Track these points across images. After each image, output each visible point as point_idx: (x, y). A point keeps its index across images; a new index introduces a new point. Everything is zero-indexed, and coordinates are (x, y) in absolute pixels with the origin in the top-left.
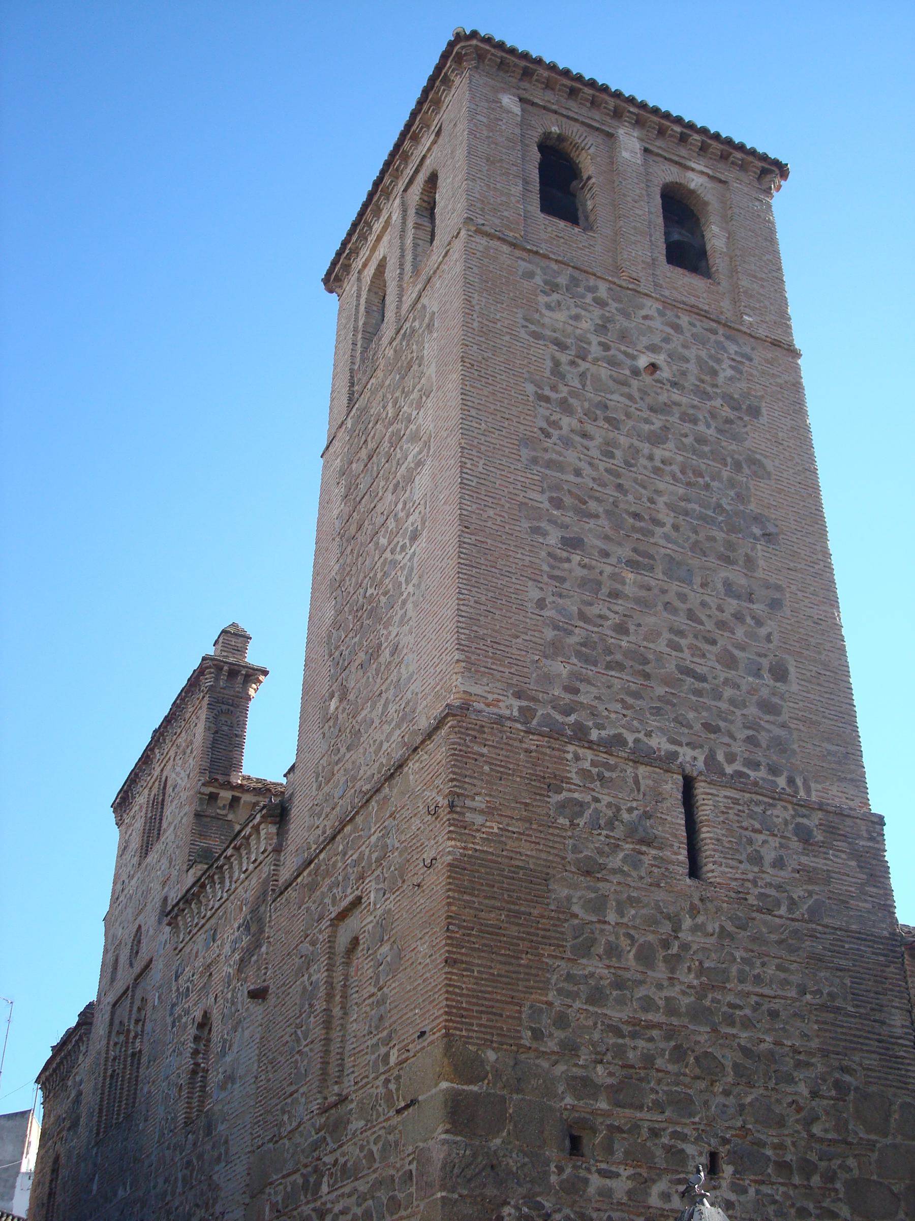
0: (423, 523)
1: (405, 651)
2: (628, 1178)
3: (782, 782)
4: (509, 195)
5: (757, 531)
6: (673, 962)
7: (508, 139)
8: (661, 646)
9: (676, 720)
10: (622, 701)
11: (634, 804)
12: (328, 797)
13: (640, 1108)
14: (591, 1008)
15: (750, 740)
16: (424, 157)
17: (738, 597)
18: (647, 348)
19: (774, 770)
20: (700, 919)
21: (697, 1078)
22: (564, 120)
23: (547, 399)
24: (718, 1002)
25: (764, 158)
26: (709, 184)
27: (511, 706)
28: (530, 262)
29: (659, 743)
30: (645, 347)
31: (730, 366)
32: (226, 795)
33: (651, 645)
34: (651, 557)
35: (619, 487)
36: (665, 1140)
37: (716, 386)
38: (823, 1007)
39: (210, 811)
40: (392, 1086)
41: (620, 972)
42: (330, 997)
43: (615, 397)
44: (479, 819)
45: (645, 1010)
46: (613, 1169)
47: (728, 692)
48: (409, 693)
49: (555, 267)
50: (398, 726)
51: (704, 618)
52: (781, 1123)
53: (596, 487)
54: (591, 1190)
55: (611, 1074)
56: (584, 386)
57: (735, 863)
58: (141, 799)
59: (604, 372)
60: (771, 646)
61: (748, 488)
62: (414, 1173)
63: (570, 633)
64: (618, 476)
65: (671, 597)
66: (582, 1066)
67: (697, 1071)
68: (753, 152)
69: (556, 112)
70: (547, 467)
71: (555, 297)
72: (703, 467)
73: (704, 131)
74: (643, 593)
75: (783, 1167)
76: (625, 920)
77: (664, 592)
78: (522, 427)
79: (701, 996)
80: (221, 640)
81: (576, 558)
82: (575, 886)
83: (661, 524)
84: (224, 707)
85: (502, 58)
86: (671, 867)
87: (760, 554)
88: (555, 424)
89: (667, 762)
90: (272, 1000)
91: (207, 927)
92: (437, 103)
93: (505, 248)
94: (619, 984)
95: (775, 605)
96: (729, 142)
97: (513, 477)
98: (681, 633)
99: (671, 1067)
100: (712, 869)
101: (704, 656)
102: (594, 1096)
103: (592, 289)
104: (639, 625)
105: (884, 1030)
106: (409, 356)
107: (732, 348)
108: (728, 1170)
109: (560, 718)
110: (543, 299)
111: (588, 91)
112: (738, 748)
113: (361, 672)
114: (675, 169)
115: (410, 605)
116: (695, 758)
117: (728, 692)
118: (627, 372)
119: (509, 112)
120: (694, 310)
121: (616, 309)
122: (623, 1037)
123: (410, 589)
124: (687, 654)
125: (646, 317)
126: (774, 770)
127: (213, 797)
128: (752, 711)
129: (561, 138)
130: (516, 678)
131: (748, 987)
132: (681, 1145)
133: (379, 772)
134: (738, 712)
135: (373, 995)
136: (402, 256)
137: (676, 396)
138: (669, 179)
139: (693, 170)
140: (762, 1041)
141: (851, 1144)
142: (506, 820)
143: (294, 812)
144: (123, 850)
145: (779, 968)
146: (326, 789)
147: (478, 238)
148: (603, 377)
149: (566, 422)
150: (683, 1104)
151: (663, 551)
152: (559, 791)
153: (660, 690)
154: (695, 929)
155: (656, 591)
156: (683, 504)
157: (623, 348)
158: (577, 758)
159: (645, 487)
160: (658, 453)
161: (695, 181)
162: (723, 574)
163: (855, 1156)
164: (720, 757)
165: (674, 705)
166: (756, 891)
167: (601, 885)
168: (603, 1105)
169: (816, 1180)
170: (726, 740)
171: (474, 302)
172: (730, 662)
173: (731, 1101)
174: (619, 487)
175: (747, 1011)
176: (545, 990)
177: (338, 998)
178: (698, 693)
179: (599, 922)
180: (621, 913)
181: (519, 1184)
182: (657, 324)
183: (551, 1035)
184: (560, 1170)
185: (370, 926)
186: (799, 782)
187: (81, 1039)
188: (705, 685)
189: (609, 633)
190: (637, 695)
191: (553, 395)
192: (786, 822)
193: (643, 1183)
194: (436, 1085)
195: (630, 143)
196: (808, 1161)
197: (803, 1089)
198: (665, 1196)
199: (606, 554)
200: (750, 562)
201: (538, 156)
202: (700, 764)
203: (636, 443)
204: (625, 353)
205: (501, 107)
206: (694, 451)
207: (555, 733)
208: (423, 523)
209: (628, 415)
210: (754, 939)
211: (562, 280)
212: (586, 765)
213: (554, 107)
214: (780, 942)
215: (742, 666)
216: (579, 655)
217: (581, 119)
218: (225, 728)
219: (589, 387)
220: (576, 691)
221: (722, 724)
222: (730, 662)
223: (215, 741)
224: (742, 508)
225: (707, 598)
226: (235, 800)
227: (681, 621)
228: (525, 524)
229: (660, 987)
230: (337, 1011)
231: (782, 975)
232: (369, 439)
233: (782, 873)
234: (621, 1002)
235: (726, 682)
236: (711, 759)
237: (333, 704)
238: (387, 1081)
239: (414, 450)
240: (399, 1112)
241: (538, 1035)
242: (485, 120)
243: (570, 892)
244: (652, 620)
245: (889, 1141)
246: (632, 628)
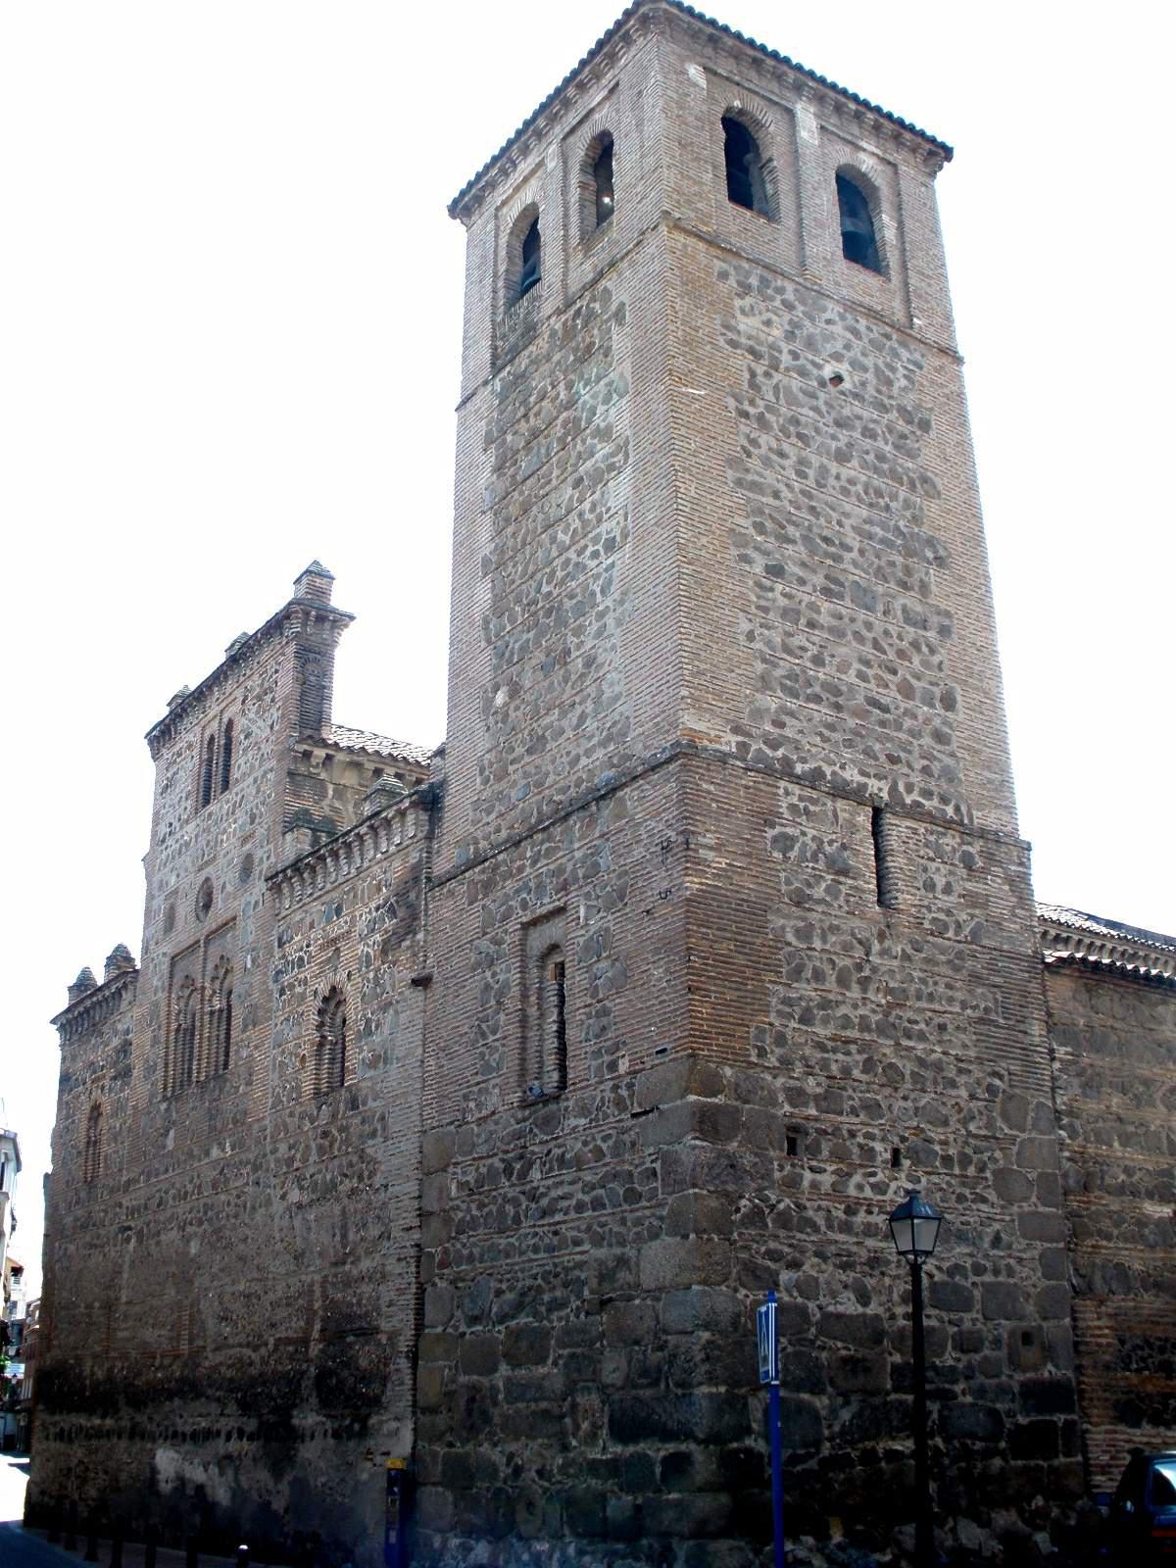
0: (625, 536)
1: (606, 668)
2: (833, 1173)
3: (950, 810)
4: (700, 183)
5: (930, 555)
6: (864, 983)
7: (697, 119)
8: (851, 677)
9: (865, 752)
10: (821, 734)
11: (834, 837)
12: (500, 797)
13: (840, 1113)
14: (804, 1028)
15: (926, 770)
16: (591, 111)
17: (914, 624)
18: (830, 356)
19: (944, 800)
20: (887, 943)
21: (882, 1086)
22: (745, 92)
23: (746, 415)
24: (901, 1018)
25: (933, 140)
26: (880, 167)
27: (730, 742)
28: (724, 261)
29: (852, 775)
30: (830, 356)
31: (905, 376)
32: (320, 753)
33: (843, 677)
34: (842, 585)
35: (812, 509)
36: (860, 1139)
37: (891, 397)
38: (981, 1021)
39: (302, 769)
40: (624, 1092)
41: (824, 994)
42: (524, 996)
43: (805, 411)
44: (711, 855)
45: (844, 1028)
46: (822, 1165)
47: (908, 723)
48: (615, 713)
49: (746, 265)
50: (603, 744)
51: (886, 647)
52: (946, 1123)
53: (792, 510)
54: (806, 1183)
55: (819, 1084)
56: (778, 399)
57: (914, 891)
58: (191, 735)
59: (796, 383)
60: (942, 675)
61: (921, 509)
62: (659, 1171)
63: (775, 666)
64: (810, 497)
65: (859, 626)
66: (797, 1079)
67: (884, 1080)
68: (922, 134)
69: (738, 84)
70: (750, 490)
71: (748, 300)
72: (883, 486)
73: (878, 110)
74: (835, 622)
75: (947, 1160)
76: (828, 947)
77: (853, 620)
78: (727, 446)
79: (887, 1015)
80: (304, 580)
81: (779, 587)
82: (787, 917)
83: (849, 549)
84: (311, 656)
85: (689, 23)
86: (864, 896)
87: (933, 578)
88: (754, 442)
89: (855, 795)
90: (437, 989)
91: (323, 899)
92: (613, 58)
93: (701, 245)
94: (825, 1005)
95: (944, 631)
96: (900, 123)
97: (721, 500)
98: (867, 663)
99: (864, 1077)
100: (905, 898)
101: (886, 686)
102: (806, 1105)
103: (780, 291)
104: (833, 656)
105: (1027, 1040)
106: (588, 340)
107: (904, 354)
108: (906, 1163)
109: (768, 751)
110: (738, 303)
111: (770, 62)
112: (916, 778)
113: (540, 675)
114: (848, 149)
115: (610, 620)
116: (880, 790)
117: (908, 723)
118: (815, 384)
119: (695, 85)
120: (873, 314)
121: (803, 313)
122: (827, 1052)
123: (609, 602)
124: (872, 685)
125: (829, 322)
126: (944, 800)
127: (307, 755)
128: (927, 741)
129: (741, 112)
130: (733, 713)
131: (924, 1004)
132: (872, 1144)
133: (578, 786)
134: (915, 743)
135: (590, 1005)
136: (566, 216)
137: (857, 408)
138: (843, 161)
139: (864, 150)
140: (933, 1051)
141: (997, 1139)
142: (732, 856)
143: (448, 801)
144: (165, 788)
145: (949, 986)
146: (497, 787)
147: (676, 235)
148: (794, 389)
149: (765, 440)
150: (872, 1109)
151: (851, 577)
152: (772, 826)
153: (852, 722)
154: (884, 952)
155: (846, 620)
156: (867, 527)
157: (810, 357)
158: (787, 793)
159: (834, 510)
160: (845, 473)
161: (867, 163)
162: (902, 601)
163: (1001, 1149)
164: (901, 788)
165: (862, 737)
166: (930, 916)
167: (808, 914)
168: (813, 1112)
169: (971, 1171)
170: (905, 770)
171: (678, 308)
172: (907, 691)
173: (909, 1104)
174: (812, 509)
175: (923, 1026)
176: (767, 1013)
177: (533, 999)
178: (883, 724)
179: (809, 949)
180: (824, 940)
181: (752, 1180)
182: (838, 329)
183: (772, 1052)
184: (781, 1168)
185: (581, 940)
186: (964, 809)
187: (125, 986)
188: (887, 716)
189: (809, 664)
190: (831, 727)
191: (752, 410)
192: (954, 850)
193: (844, 1176)
194: (683, 1097)
195: (807, 117)
196: (965, 1154)
197: (964, 1094)
198: (860, 1187)
199: (802, 582)
200: (924, 588)
201: (723, 135)
202: (885, 795)
203: (825, 461)
204: (813, 363)
205: (689, 80)
206: (876, 470)
207: (769, 771)
208: (625, 536)
209: (817, 430)
210: (927, 960)
211: (754, 281)
212: (795, 800)
213: (737, 78)
214: (949, 962)
215: (918, 695)
216: (784, 688)
217: (762, 92)
218: (312, 678)
219: (782, 401)
220: (782, 725)
221: (903, 755)
222: (907, 691)
223: (303, 694)
224: (916, 530)
225: (890, 628)
226: (329, 757)
227: (868, 650)
228: (734, 552)
229: (855, 1007)
230: (533, 1011)
231: (950, 993)
232: (531, 414)
233: (951, 899)
234: (825, 1021)
235: (906, 712)
236: (893, 789)
237: (500, 698)
238: (616, 1088)
239: (603, 450)
240: (634, 1116)
241: (762, 1053)
242: (675, 96)
243: (785, 923)
244: (843, 650)
245: (1025, 1136)
246: (828, 659)
